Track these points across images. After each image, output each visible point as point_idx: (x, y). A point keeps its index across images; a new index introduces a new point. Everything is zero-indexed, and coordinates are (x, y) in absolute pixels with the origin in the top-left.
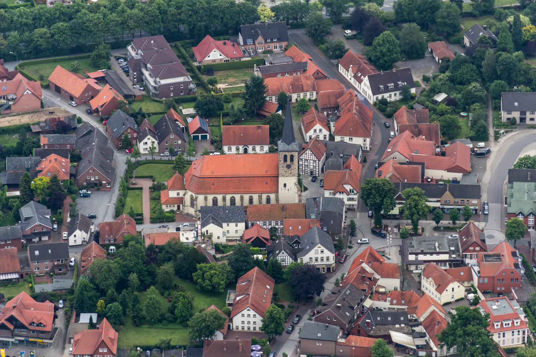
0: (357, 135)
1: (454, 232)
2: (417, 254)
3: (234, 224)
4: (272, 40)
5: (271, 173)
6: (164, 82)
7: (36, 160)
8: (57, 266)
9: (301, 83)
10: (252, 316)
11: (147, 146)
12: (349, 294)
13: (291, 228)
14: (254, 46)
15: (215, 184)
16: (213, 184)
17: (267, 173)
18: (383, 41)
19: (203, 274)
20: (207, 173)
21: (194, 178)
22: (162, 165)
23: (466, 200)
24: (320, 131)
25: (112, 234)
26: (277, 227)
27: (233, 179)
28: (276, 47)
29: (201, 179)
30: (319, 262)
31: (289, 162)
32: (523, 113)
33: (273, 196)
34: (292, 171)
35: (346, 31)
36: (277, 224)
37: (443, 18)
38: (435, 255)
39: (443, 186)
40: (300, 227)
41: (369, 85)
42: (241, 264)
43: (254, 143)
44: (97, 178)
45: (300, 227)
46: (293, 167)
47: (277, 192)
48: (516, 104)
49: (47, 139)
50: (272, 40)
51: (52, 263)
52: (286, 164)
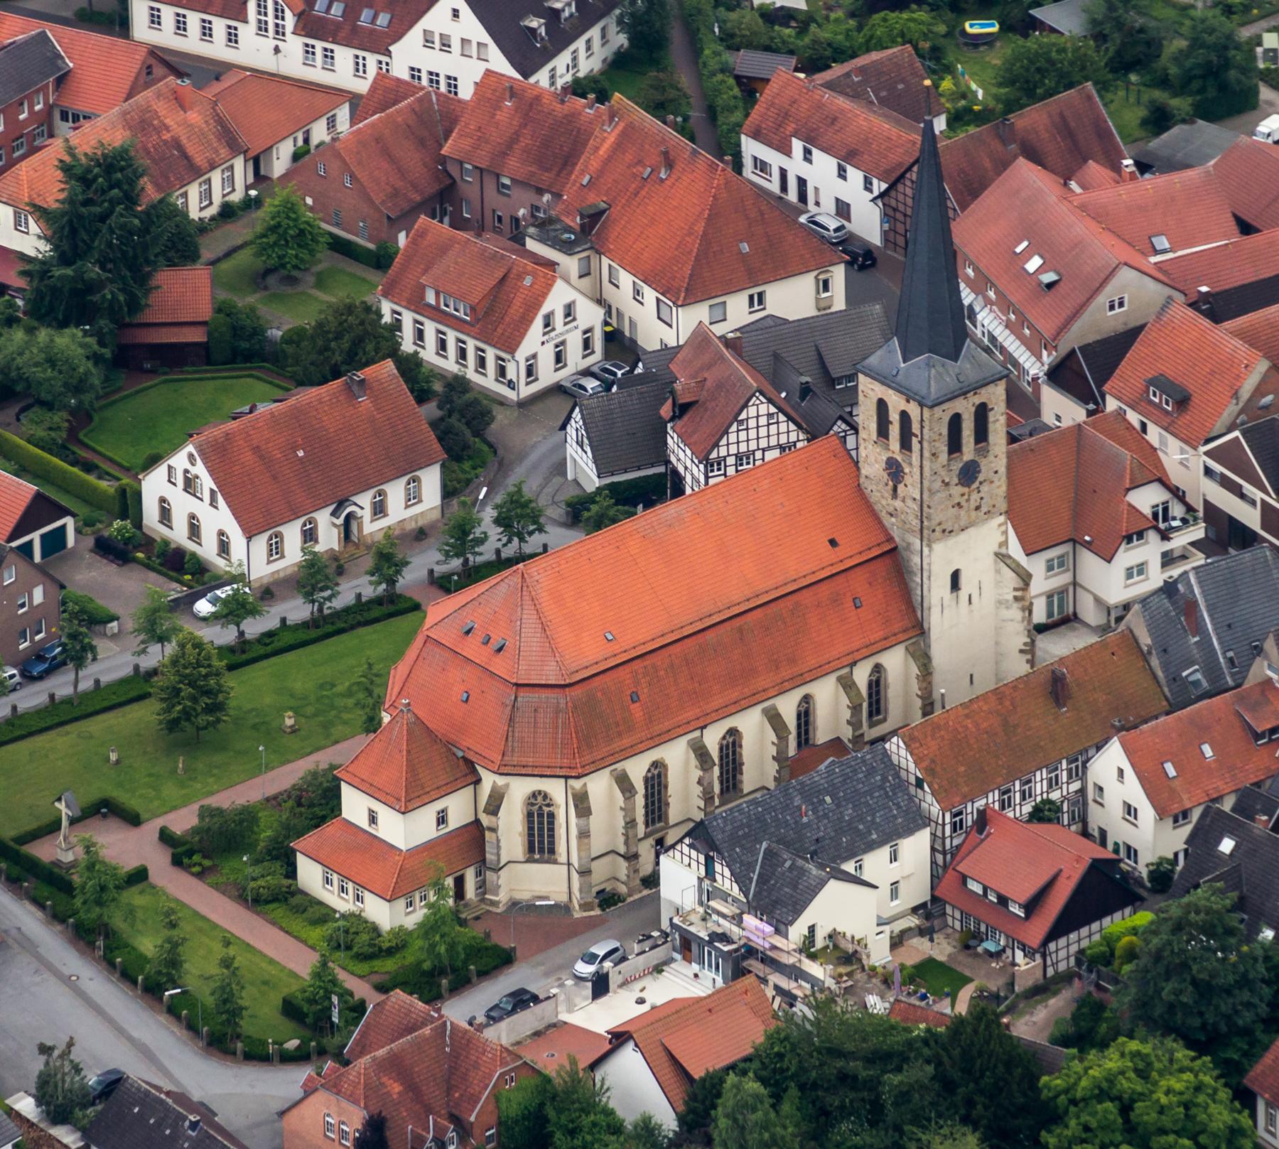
0: (783, 270)
5: (854, 547)
9: (166, 136)
13: (1170, 770)
15: (644, 693)
16: (634, 698)
19: (1126, 1109)
25: (429, 1110)
26: (1055, 796)
27: (710, 635)
29: (577, 692)
31: (968, 448)
33: (895, 661)
34: (985, 488)
36: (1053, 783)
40: (1207, 750)
41: (485, 37)
42: (1225, 1006)
45: (1207, 750)
47: (915, 630)
52: (957, 466)
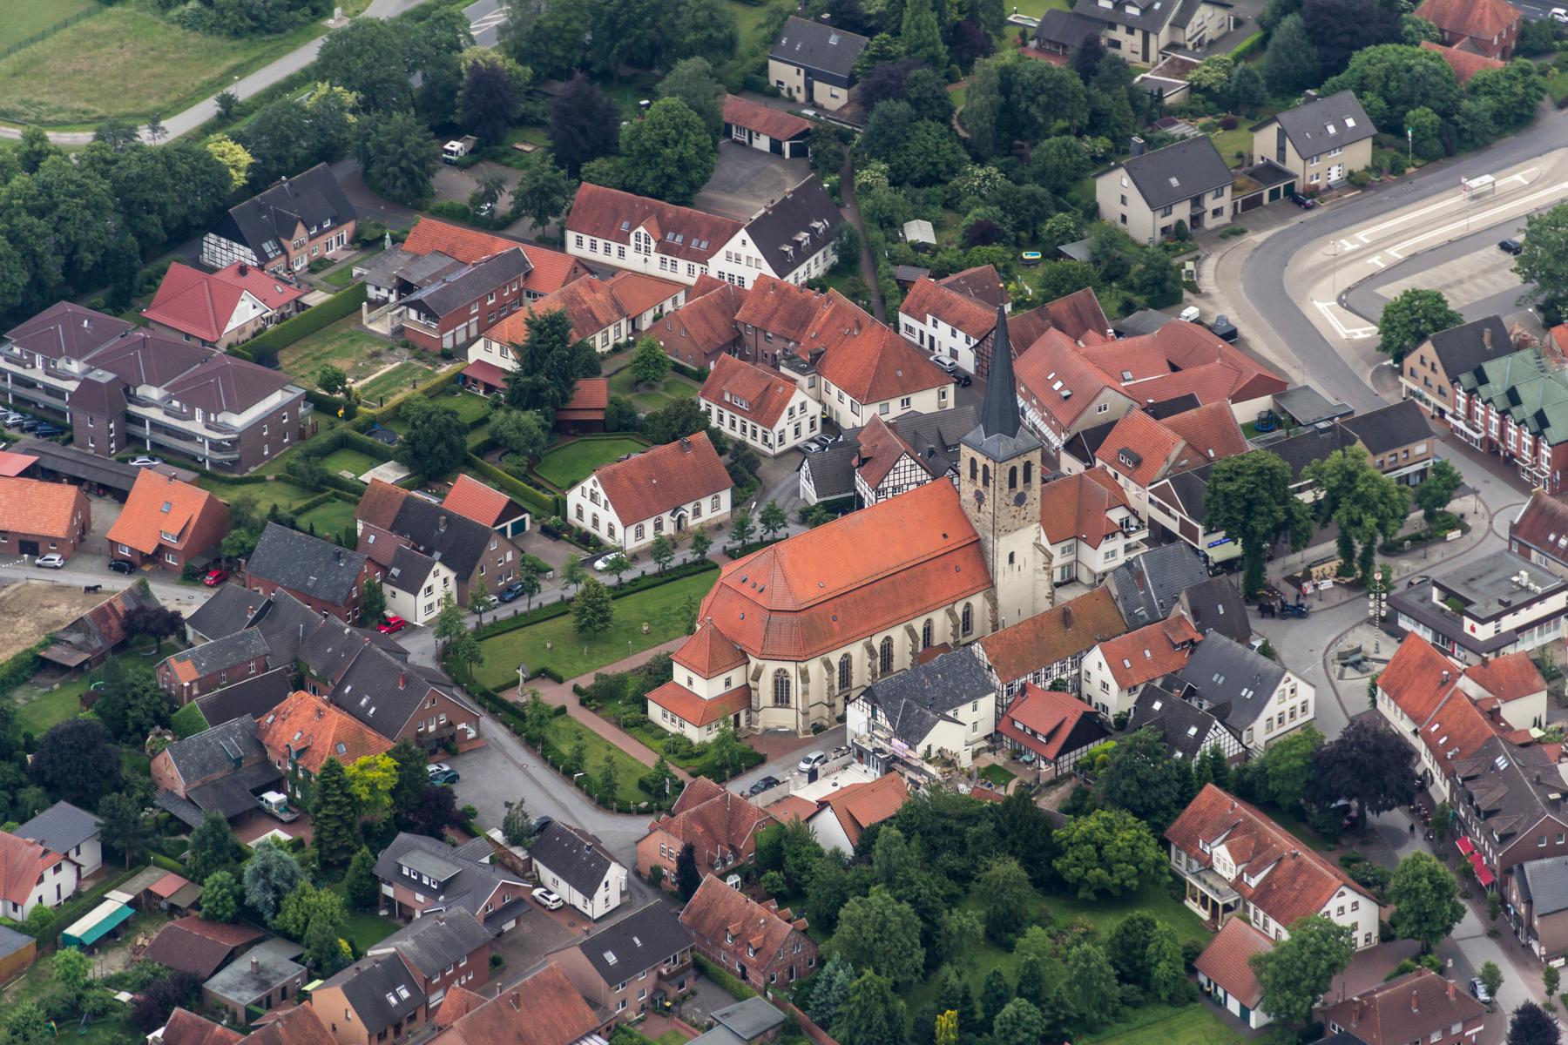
0: (921, 387)
1: (1436, 543)
2: (1497, 617)
3: (970, 705)
4: (320, 226)
6: (239, 421)
7: (243, 728)
8: (672, 976)
10: (1348, 909)
11: (433, 598)
12: (1494, 767)
14: (283, 259)
15: (840, 617)
17: (950, 540)
18: (676, 128)
20: (809, 592)
21: (775, 617)
22: (519, 636)
23: (1400, 451)
24: (803, 406)
25: (718, 842)
26: (1064, 677)
27: (876, 585)
28: (328, 246)
29: (803, 615)
30: (1288, 725)
32: (1197, 202)
33: (978, 602)
35: (447, 147)
36: (1063, 670)
37: (697, 28)
38: (1537, 606)
39: (1329, 434)
40: (1148, 653)
43: (695, 495)
44: (443, 719)
45: (1148, 653)
46: (1030, 496)
48: (1174, 182)
49: (189, 664)
50: (320, 226)
51: (653, 975)
52: (1013, 495)
